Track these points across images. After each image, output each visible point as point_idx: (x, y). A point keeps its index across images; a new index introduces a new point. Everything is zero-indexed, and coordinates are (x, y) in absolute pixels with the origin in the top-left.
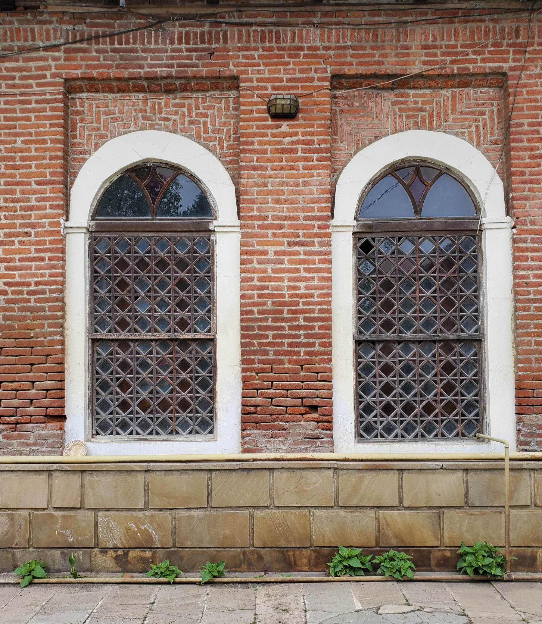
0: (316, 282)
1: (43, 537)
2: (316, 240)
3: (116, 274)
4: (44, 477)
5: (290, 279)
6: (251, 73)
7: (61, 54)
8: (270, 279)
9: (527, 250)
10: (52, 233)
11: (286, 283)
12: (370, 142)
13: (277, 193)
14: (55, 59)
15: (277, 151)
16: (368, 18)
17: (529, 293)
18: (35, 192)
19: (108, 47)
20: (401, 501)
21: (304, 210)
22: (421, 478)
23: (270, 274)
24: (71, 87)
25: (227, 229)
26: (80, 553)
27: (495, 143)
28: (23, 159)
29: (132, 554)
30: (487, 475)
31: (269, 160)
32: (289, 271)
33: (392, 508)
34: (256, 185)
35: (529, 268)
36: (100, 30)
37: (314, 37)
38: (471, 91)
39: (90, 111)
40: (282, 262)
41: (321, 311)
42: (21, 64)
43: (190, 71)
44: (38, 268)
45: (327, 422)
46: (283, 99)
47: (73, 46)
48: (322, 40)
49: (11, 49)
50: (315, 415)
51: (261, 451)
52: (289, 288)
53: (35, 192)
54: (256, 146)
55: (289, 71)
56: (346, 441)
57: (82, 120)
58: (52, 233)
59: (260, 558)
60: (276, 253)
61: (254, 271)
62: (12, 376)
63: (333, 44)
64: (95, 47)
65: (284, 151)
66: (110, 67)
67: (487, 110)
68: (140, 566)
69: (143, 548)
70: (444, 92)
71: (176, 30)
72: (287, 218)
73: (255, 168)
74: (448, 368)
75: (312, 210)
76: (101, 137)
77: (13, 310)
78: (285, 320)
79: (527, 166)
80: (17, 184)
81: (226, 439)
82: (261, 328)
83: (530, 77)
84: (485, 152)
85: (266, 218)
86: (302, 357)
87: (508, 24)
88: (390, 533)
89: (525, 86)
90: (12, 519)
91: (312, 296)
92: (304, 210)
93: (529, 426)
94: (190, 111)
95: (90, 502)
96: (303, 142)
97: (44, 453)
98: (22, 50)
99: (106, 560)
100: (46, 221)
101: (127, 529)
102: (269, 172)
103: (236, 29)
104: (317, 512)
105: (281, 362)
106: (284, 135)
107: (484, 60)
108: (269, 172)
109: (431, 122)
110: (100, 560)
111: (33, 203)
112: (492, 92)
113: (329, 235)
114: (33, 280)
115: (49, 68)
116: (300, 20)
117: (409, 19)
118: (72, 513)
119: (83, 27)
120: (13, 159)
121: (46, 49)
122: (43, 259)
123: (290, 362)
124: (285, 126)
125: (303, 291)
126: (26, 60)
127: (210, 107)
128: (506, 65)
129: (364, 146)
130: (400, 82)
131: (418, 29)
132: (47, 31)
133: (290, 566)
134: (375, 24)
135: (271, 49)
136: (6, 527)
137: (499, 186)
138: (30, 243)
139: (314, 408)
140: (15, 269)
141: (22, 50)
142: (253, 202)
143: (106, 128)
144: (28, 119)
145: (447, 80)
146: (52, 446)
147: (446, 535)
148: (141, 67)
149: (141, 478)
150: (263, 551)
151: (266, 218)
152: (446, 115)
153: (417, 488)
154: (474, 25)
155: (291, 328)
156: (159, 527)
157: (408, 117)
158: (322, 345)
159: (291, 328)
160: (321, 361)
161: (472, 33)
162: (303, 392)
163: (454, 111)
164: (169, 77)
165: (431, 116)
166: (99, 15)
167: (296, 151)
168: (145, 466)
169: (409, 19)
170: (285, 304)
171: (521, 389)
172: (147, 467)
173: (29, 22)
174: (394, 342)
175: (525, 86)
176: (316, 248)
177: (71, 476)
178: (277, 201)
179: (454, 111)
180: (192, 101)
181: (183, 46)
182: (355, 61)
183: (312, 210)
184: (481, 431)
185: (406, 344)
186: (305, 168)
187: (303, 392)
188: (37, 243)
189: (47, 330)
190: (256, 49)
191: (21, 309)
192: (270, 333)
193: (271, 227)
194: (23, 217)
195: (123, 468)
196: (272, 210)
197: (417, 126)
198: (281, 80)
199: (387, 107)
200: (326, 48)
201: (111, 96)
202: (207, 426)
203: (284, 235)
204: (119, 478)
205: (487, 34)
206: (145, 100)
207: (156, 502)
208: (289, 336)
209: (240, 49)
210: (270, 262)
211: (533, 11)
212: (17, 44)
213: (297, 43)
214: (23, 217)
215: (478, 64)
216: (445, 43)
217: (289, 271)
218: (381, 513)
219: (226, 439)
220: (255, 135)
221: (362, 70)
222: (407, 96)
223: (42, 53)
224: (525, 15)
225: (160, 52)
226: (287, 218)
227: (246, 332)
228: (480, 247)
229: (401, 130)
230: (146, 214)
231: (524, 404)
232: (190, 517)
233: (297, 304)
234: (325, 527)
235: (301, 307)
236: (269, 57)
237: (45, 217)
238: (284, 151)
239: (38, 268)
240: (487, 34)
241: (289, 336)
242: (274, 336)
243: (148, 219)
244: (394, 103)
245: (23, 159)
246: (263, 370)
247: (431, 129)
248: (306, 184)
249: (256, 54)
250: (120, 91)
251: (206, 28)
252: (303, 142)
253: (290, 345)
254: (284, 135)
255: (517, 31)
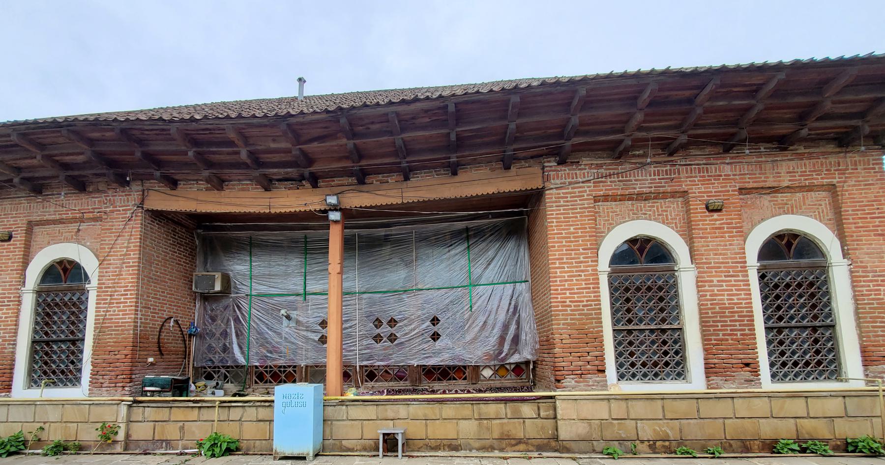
0: (743, 296)
1: (608, 435)
2: (740, 274)
3: (623, 294)
4: (605, 402)
5: (728, 295)
6: (694, 189)
7: (592, 184)
8: (716, 295)
9: (860, 276)
10: (593, 275)
11: (726, 297)
12: (759, 223)
13: (715, 250)
14: (588, 187)
15: (713, 228)
16: (755, 159)
17: (864, 300)
18: (582, 254)
19: (616, 179)
20: (808, 414)
21: (731, 258)
22: (819, 401)
23: (716, 292)
24: (596, 199)
25: (686, 270)
26: (629, 443)
27: (830, 220)
28: (574, 237)
29: (658, 443)
30: (856, 399)
31: (709, 233)
32: (727, 290)
33: (803, 418)
34: (703, 246)
35: (862, 286)
36: (612, 171)
37: (727, 170)
38: (813, 193)
39: (604, 211)
40: (722, 286)
41: (747, 312)
42: (570, 190)
43: (661, 190)
44: (587, 293)
45: (756, 372)
46: (715, 201)
47: (598, 180)
48: (732, 171)
49: (564, 183)
50: (747, 369)
51: (721, 388)
52: (728, 300)
53: (582, 254)
54: (701, 226)
55: (715, 187)
56: (767, 383)
57: (600, 216)
58: (593, 275)
59: (731, 446)
60: (718, 281)
61: (707, 291)
62: (577, 350)
63: (738, 173)
64: (609, 180)
65: (716, 228)
66: (618, 189)
67: (823, 203)
68: (663, 450)
69: (664, 441)
70: (798, 194)
71: (652, 169)
72: (722, 263)
73: (701, 238)
74: (816, 341)
75: (736, 258)
76: (611, 224)
77: (575, 315)
78: (727, 317)
79: (854, 232)
80: (572, 250)
81: (696, 380)
82: (714, 322)
83: (849, 186)
84: (826, 224)
85: (710, 263)
86: (739, 336)
87: (833, 159)
88: (804, 432)
89: (847, 191)
90: (590, 425)
91: (741, 303)
92: (731, 258)
93: (873, 372)
94: (658, 209)
95: (632, 416)
96: (727, 224)
97: (598, 390)
98: (570, 183)
99: (643, 447)
100: (590, 269)
101: (654, 430)
102: (709, 239)
103: (684, 167)
104: (761, 421)
105: (727, 340)
106: (716, 220)
107: (822, 178)
108: (709, 239)
109: (792, 210)
110: (641, 447)
111: (582, 259)
112: (824, 194)
113: (747, 271)
114: (585, 299)
115: (585, 191)
116: (719, 162)
117: (778, 159)
118: (623, 421)
119: (602, 171)
120: (569, 238)
121: (583, 182)
122: (589, 288)
123: (732, 339)
124: (716, 215)
125: (736, 301)
126: (573, 188)
127: (670, 207)
128: (835, 181)
129: (756, 225)
130: (774, 190)
131: (784, 163)
132: (584, 174)
133: (747, 449)
134: (759, 162)
135: (704, 176)
136: (587, 429)
137: (837, 244)
138: (582, 280)
139: (747, 365)
140: (575, 293)
141: (570, 183)
142: (702, 255)
143: (613, 219)
144: (576, 217)
145: (802, 188)
146: (602, 386)
147: (837, 433)
148: (635, 188)
149: (660, 402)
150: (732, 442)
151: (710, 263)
152: (801, 206)
153: (817, 407)
154: (815, 161)
155: (731, 321)
156: (672, 429)
157: (779, 208)
158: (749, 330)
159: (731, 321)
160: (750, 339)
161: (814, 165)
162: (742, 356)
163: (804, 204)
164: (651, 193)
165: (792, 207)
166: (610, 164)
167: (723, 228)
168: (662, 396)
169: (778, 159)
170: (727, 308)
171: (864, 351)
172: (662, 397)
173: (574, 169)
174: (784, 328)
175: (847, 191)
176: (741, 278)
177: (620, 402)
178: (716, 254)
179: (804, 204)
180: (659, 204)
181: (657, 177)
182: (751, 181)
183: (736, 258)
184: (840, 375)
185: (791, 328)
186: (729, 237)
187: (742, 356)
188: (586, 280)
189: (594, 325)
190: (696, 177)
191: (579, 315)
192: (719, 324)
193: (714, 267)
194: (577, 267)
195: (649, 398)
196: (713, 259)
197: (785, 213)
198: (711, 192)
199: (766, 203)
200: (734, 175)
201: (614, 203)
202: (681, 374)
203: (722, 272)
204: (647, 402)
205: (822, 165)
206: (633, 205)
207: (669, 416)
208: (730, 326)
209: (687, 177)
210: (715, 286)
211: (846, 152)
212: (567, 180)
213: (718, 173)
214: (577, 267)
215: (819, 180)
216: (799, 170)
217: (727, 290)
218: (798, 420)
219: (696, 380)
220: (701, 220)
221: (755, 185)
222: (777, 197)
223: (581, 185)
224: (842, 155)
225: (644, 179)
226: (722, 263)
227: (704, 324)
228: (828, 276)
229: (776, 215)
230: (637, 263)
231: (868, 359)
232: (689, 423)
233: (733, 308)
234: (767, 429)
235: (736, 309)
236: (703, 181)
237: (589, 266)
238: (716, 228)
239: (587, 293)
240: (822, 165)
241: (730, 326)
242: (722, 326)
243: (638, 266)
244: (770, 201)
245: (574, 237)
246: (718, 345)
247: (793, 213)
248: (731, 245)
249: (696, 179)
250: (620, 200)
251: (668, 168)
252: (727, 224)
253: (731, 330)
254: (716, 220)
255: (839, 163)
